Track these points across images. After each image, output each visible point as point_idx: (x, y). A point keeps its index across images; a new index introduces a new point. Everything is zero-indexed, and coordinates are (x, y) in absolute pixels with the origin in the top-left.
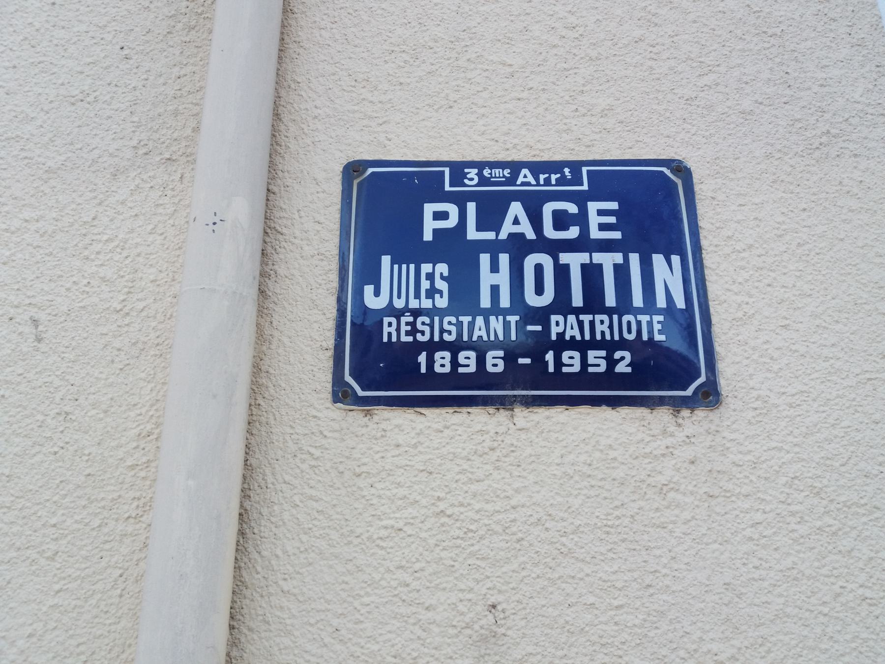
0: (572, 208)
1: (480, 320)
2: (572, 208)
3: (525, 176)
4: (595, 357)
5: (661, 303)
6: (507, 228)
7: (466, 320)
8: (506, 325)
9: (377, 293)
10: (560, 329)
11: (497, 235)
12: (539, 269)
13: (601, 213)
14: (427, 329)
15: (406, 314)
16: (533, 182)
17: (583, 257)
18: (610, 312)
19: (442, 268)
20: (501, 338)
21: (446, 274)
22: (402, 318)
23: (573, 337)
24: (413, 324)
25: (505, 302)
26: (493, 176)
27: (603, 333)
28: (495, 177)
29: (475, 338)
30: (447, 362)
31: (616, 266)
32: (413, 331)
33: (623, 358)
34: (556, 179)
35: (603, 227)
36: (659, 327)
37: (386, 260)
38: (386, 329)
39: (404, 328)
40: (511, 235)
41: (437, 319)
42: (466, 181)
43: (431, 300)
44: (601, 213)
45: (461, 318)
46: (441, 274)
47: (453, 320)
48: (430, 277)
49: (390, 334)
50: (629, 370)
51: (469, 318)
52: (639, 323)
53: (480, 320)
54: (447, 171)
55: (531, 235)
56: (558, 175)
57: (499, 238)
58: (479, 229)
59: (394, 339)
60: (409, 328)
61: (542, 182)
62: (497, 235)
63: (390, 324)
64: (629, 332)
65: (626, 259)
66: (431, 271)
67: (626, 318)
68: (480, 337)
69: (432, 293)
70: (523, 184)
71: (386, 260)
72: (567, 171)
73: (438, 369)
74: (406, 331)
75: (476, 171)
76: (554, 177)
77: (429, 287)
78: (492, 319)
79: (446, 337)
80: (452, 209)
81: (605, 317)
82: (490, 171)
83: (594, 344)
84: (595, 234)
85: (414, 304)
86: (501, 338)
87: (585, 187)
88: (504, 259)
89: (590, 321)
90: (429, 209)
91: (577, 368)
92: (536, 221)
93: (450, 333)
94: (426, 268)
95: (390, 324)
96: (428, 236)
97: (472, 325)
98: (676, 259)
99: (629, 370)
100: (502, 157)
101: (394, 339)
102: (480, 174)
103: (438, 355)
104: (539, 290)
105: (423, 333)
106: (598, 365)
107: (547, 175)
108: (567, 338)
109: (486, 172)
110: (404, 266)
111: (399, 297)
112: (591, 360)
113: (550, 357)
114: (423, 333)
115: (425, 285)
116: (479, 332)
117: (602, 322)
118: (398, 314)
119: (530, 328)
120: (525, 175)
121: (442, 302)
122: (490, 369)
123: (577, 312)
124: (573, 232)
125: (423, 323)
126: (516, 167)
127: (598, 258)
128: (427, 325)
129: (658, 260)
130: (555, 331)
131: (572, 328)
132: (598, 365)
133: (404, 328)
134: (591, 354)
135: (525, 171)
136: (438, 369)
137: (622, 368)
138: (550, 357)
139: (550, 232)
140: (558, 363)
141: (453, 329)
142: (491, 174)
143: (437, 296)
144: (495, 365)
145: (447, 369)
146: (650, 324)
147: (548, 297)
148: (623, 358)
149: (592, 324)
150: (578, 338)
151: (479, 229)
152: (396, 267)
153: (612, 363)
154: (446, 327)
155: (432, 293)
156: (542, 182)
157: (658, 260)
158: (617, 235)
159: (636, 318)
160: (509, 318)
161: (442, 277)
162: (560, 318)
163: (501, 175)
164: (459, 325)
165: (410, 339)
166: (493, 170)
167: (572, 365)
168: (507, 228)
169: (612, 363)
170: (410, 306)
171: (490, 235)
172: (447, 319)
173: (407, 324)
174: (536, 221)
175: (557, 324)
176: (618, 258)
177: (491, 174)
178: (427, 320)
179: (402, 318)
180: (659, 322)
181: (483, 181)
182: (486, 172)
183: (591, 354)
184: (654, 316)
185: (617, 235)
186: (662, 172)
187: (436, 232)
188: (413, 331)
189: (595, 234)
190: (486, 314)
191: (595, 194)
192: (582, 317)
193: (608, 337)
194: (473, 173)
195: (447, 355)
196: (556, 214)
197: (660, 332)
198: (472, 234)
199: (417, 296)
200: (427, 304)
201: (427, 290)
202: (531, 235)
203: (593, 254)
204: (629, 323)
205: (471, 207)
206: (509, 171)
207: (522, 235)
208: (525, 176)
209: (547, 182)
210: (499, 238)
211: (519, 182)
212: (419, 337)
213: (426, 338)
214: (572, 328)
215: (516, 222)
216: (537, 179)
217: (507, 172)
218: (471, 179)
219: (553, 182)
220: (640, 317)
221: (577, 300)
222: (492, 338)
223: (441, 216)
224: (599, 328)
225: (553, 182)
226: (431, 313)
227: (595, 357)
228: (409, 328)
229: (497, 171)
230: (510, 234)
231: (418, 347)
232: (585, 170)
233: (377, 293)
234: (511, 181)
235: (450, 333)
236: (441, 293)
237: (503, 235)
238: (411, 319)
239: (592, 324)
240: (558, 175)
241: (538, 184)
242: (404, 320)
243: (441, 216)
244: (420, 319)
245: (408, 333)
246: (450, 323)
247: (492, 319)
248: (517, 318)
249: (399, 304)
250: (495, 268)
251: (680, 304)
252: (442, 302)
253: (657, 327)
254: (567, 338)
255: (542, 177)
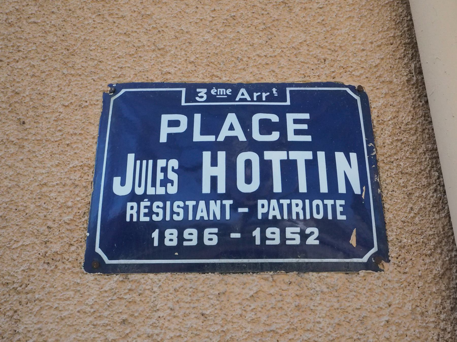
0: (274, 118)
1: (202, 204)
2: (274, 118)
3: (243, 94)
4: (291, 233)
5: (342, 189)
6: (224, 133)
7: (191, 204)
8: (223, 207)
9: (123, 183)
10: (265, 210)
11: (216, 138)
12: (248, 163)
13: (296, 121)
14: (161, 211)
15: (145, 200)
16: (249, 99)
17: (282, 155)
18: (303, 197)
19: (174, 163)
20: (218, 217)
21: (176, 167)
22: (142, 203)
23: (275, 217)
24: (150, 208)
25: (221, 189)
26: (219, 94)
27: (298, 214)
28: (220, 95)
29: (198, 218)
30: (277, 237)
31: (307, 161)
32: (150, 213)
33: (312, 233)
34: (266, 97)
35: (297, 132)
36: (341, 209)
37: (131, 157)
38: (129, 212)
39: (143, 211)
40: (227, 138)
41: (168, 203)
42: (197, 99)
43: (164, 188)
44: (296, 121)
45: (187, 203)
46: (173, 168)
47: (181, 204)
48: (164, 170)
49: (132, 216)
50: (317, 242)
51: (194, 203)
52: (325, 206)
53: (202, 204)
54: (184, 90)
55: (242, 138)
56: (268, 94)
57: (218, 140)
58: (202, 134)
59: (135, 219)
60: (146, 211)
61: (255, 99)
62: (216, 138)
63: (132, 208)
64: (318, 213)
65: (315, 156)
66: (165, 165)
67: (315, 202)
68: (202, 218)
69: (164, 183)
70: (241, 100)
71: (131, 157)
72: (274, 90)
73: (167, 243)
74: (145, 213)
75: (205, 90)
76: (264, 95)
77: (163, 178)
78: (212, 202)
79: (175, 217)
80: (183, 119)
81: (300, 202)
82: (216, 91)
83: (293, 223)
84: (291, 137)
85: (151, 191)
86: (218, 217)
87: (288, 103)
88: (222, 156)
89: (332, 205)
90: (165, 118)
91: (277, 242)
92: (247, 128)
93: (178, 214)
94: (161, 163)
95: (132, 208)
96: (163, 139)
97: (195, 208)
98: (353, 156)
99: (317, 242)
100: (225, 79)
101: (135, 219)
102: (208, 93)
103: (168, 232)
104: (248, 180)
105: (157, 214)
106: (294, 239)
107: (259, 94)
108: (270, 217)
109: (213, 92)
110: (144, 162)
111: (140, 186)
112: (288, 235)
113: (257, 233)
114: (157, 214)
115: (160, 176)
116: (202, 213)
117: (297, 205)
118: (137, 199)
119: (241, 210)
120: (243, 93)
121: (173, 190)
122: (207, 242)
123: (278, 197)
124: (275, 136)
125: (158, 207)
126: (236, 88)
127: (294, 155)
128: (182, 208)
129: (340, 156)
130: (261, 211)
131: (274, 210)
132: (294, 239)
133: (143, 211)
134: (289, 230)
135: (243, 90)
136: (167, 243)
137: (312, 241)
138: (257, 233)
139: (257, 136)
140: (264, 238)
141: (181, 211)
142: (217, 93)
143: (169, 185)
144: (211, 239)
145: (175, 243)
146: (334, 207)
147: (255, 186)
148: (312, 233)
149: (289, 206)
150: (279, 217)
151: (202, 134)
152: (138, 162)
153: (304, 236)
154: (176, 209)
155: (165, 182)
156: (255, 99)
157: (340, 156)
158: (308, 138)
159: (278, 202)
160: (224, 202)
161: (173, 170)
162: (265, 202)
163: (225, 94)
164: (186, 208)
165: (147, 219)
166: (219, 90)
167: (274, 239)
168: (224, 133)
169: (304, 236)
170: (149, 193)
171: (211, 138)
172: (176, 203)
173: (146, 207)
174: (247, 128)
175: (263, 206)
176: (309, 155)
177: (217, 93)
178: (161, 204)
179: (142, 203)
180: (341, 206)
181: (211, 98)
182: (213, 92)
183: (289, 230)
184: (337, 201)
185: (308, 138)
186: (346, 91)
187: (169, 135)
188: (150, 213)
189: (291, 137)
190: (207, 198)
191: (292, 109)
192: (282, 201)
193: (301, 217)
194: (203, 92)
195: (175, 232)
196: (262, 122)
197: (342, 213)
198: (197, 137)
199: (154, 184)
200: (161, 191)
201: (161, 180)
202: (242, 138)
203: (290, 152)
204: (318, 206)
205: (197, 117)
206: (230, 90)
207: (236, 137)
208: (243, 94)
209: (259, 99)
210: (218, 140)
211: (237, 99)
212: (155, 218)
213: (160, 218)
214: (274, 210)
215: (231, 128)
216: (251, 96)
217: (229, 91)
218: (202, 97)
219: (264, 99)
220: (326, 202)
221: (277, 188)
222: (211, 218)
223: (174, 124)
224: (295, 210)
225: (264, 99)
226: (164, 198)
227: (291, 233)
228: (146, 211)
229: (222, 90)
230: (226, 137)
231: (152, 225)
232: (288, 89)
233: (123, 183)
234: (232, 98)
235: (178, 214)
236: (172, 182)
237: (221, 138)
238: (148, 204)
239: (289, 206)
240: (268, 94)
241: (252, 100)
242: (143, 204)
243: (174, 124)
244: (156, 204)
245: (145, 215)
246: (178, 207)
247: (212, 202)
248: (231, 202)
249: (139, 191)
250: (214, 163)
251: (357, 190)
252: (173, 190)
253: (339, 209)
254: (270, 217)
255: (255, 95)
